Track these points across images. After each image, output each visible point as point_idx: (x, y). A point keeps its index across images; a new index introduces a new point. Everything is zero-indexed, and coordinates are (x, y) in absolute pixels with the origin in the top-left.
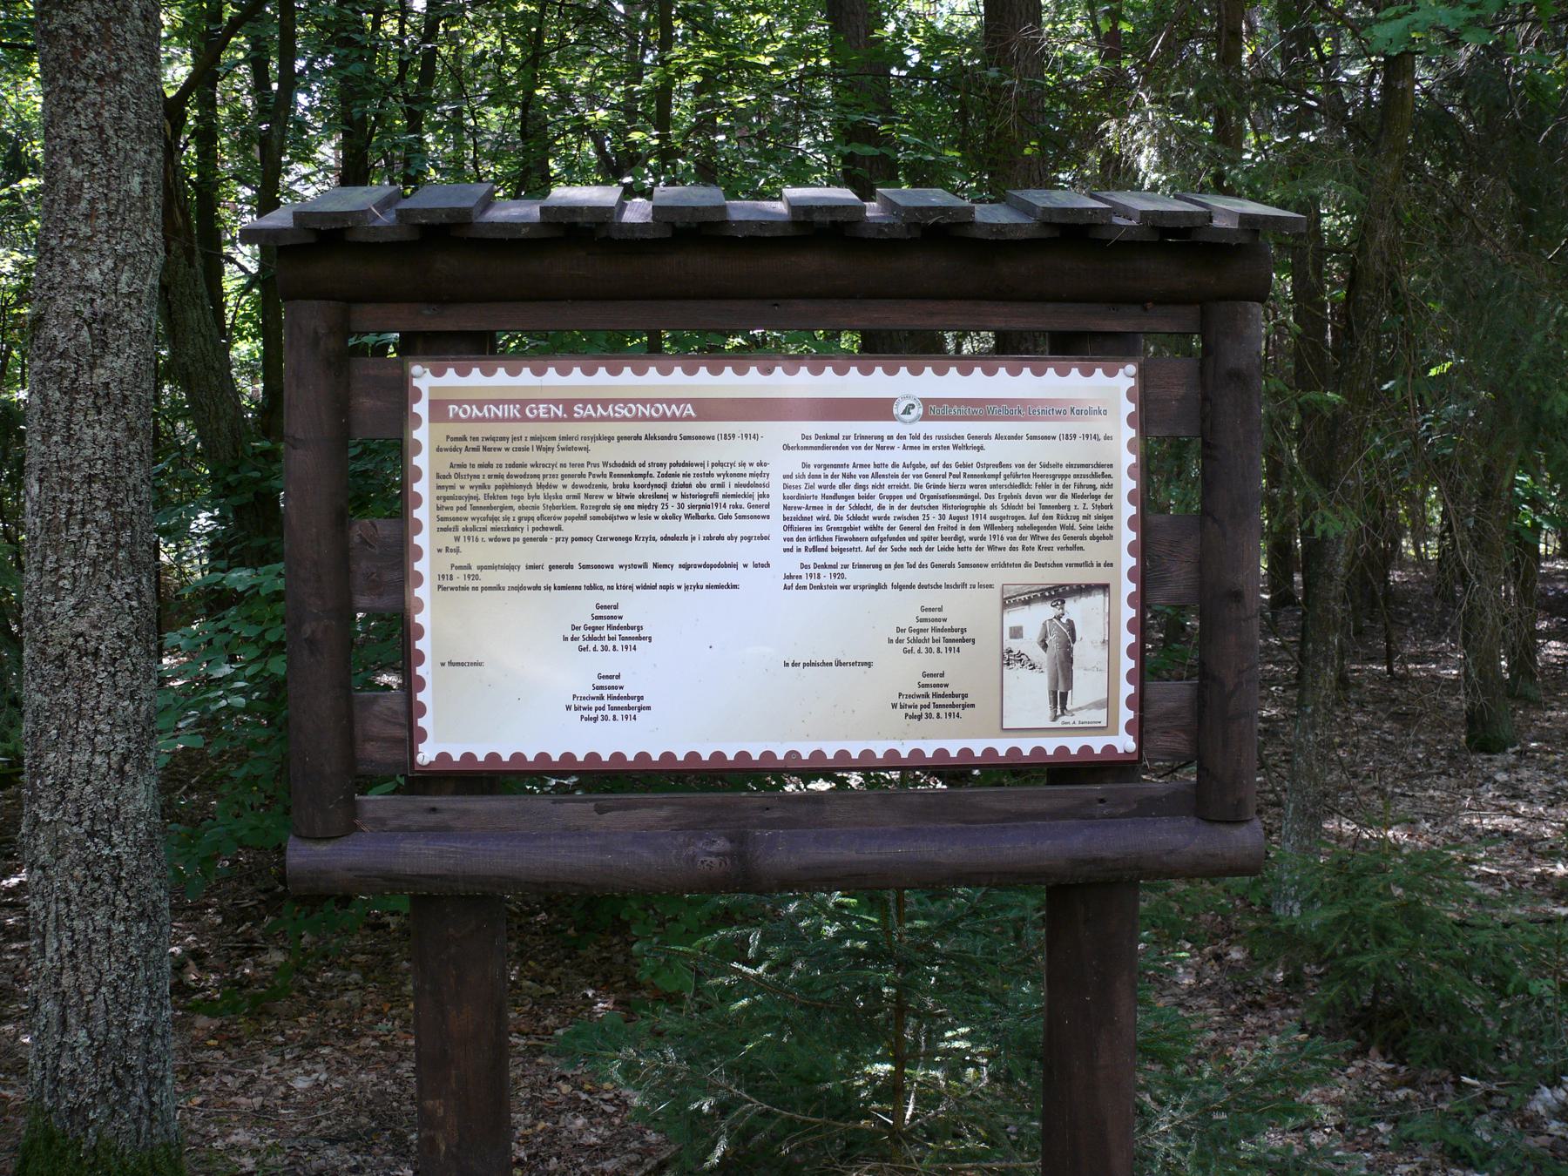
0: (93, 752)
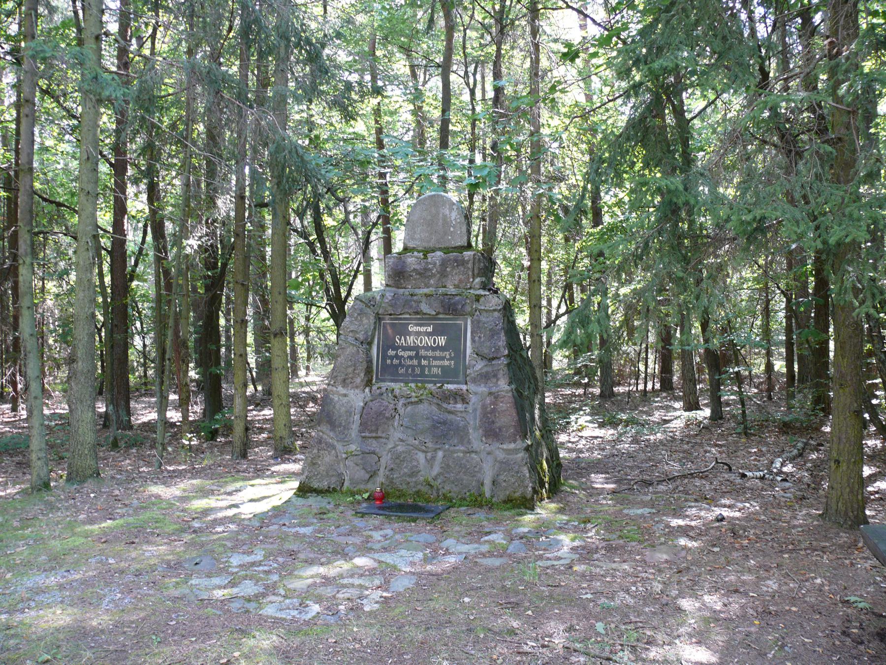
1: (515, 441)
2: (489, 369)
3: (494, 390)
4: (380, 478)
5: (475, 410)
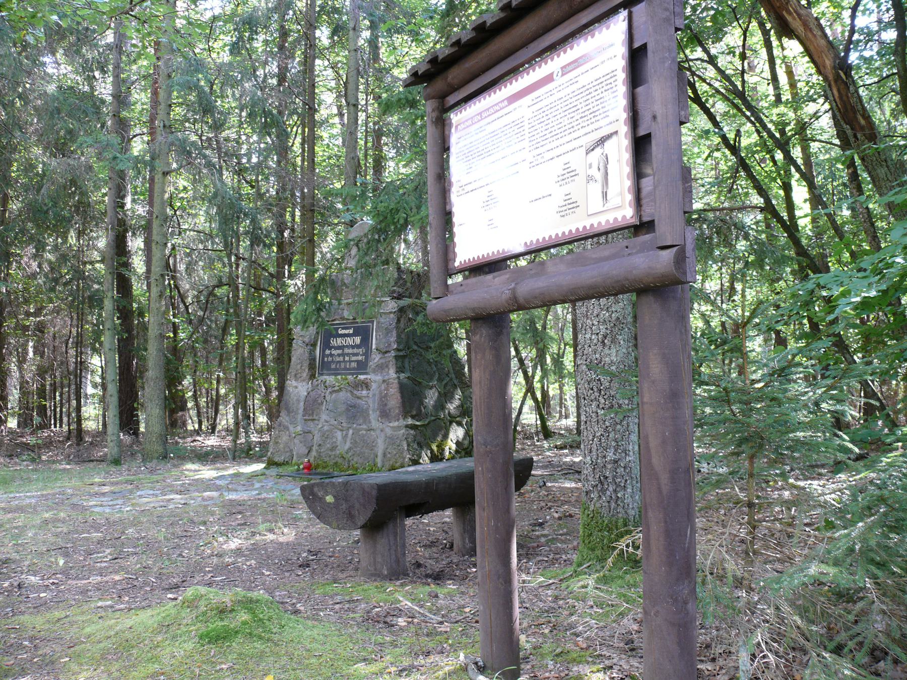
0: (592, 334)
1: (398, 420)
2: (383, 361)
3: (386, 378)
4: (314, 453)
5: (374, 395)
